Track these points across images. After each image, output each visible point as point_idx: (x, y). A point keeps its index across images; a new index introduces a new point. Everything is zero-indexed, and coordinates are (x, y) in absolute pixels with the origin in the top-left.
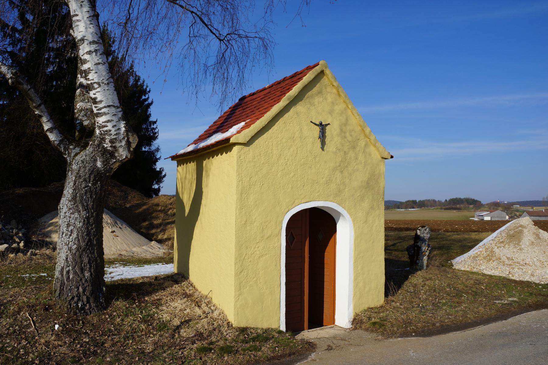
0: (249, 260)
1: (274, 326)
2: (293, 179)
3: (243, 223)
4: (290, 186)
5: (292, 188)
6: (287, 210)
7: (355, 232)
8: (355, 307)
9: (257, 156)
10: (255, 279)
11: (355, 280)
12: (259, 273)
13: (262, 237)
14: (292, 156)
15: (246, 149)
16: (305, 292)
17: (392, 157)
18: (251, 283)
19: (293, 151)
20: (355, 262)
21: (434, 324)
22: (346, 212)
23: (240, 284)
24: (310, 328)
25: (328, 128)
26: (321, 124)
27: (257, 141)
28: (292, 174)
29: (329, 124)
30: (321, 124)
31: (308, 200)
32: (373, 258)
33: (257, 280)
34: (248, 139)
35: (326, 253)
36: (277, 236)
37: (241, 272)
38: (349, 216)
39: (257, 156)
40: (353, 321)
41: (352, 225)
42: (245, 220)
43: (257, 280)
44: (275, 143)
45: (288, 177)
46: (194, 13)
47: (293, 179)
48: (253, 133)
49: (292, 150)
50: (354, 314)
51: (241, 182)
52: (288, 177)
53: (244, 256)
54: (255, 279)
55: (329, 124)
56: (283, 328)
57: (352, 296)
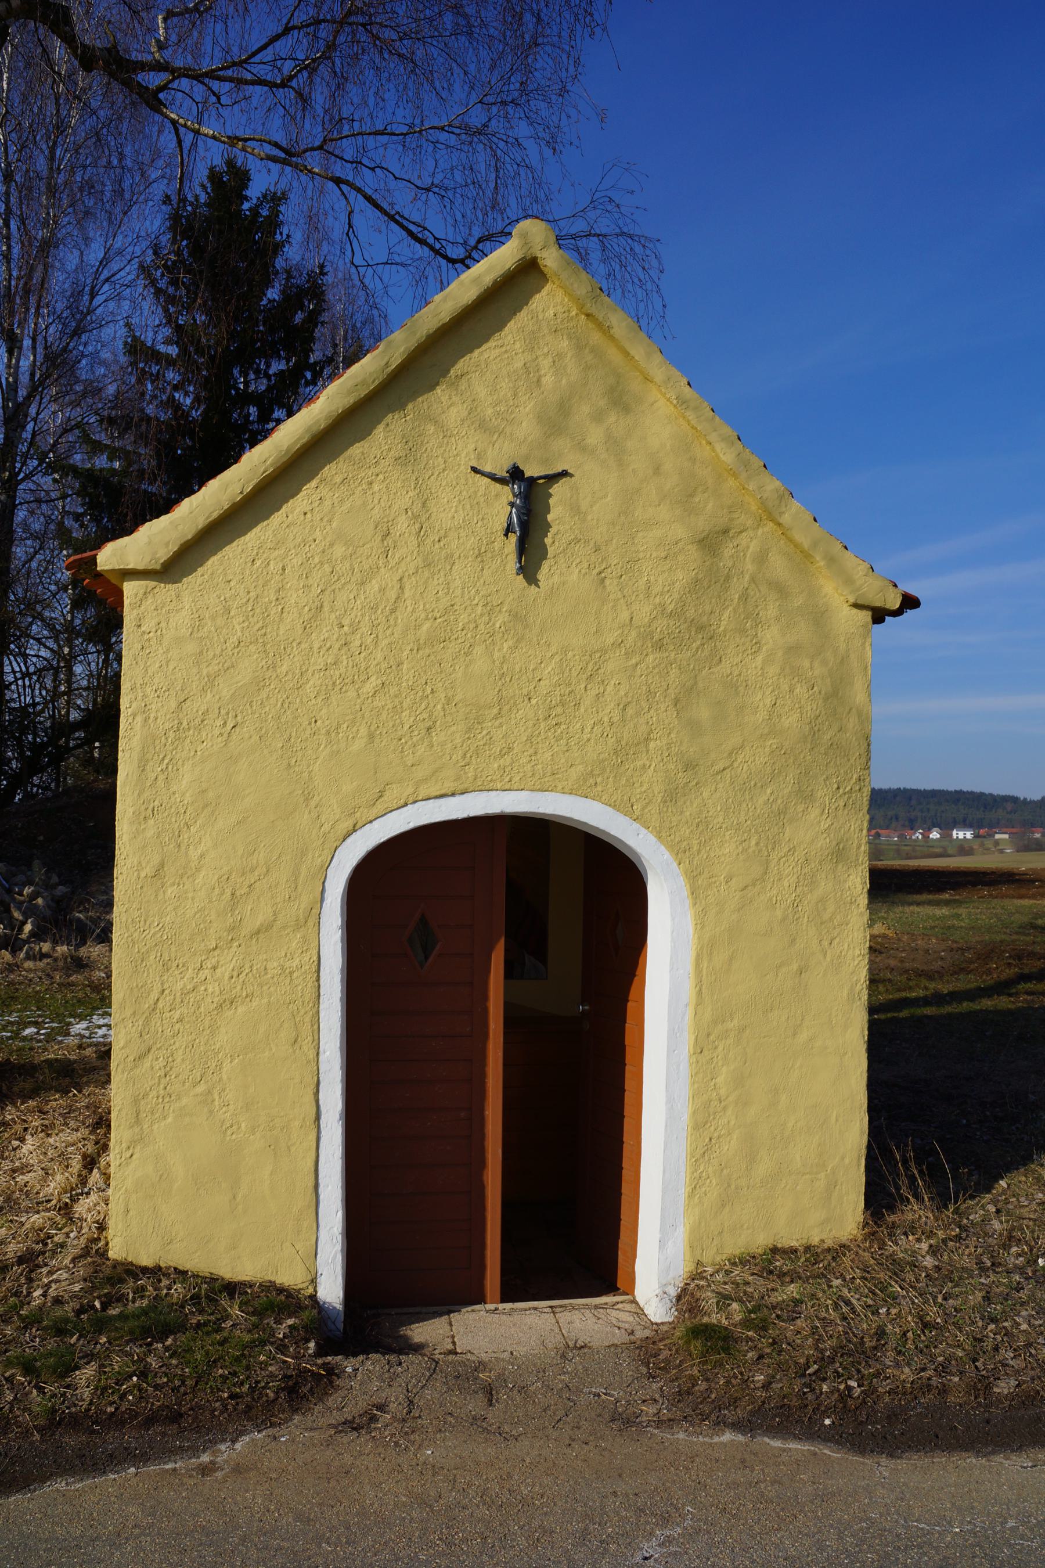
0: (177, 1015)
1: (290, 1277)
2: (378, 703)
3: (148, 871)
4: (363, 731)
5: (371, 737)
6: (348, 824)
7: (701, 924)
8: (695, 1242)
9: (213, 618)
10: (201, 1088)
11: (699, 1125)
12: (220, 1067)
13: (232, 929)
14: (374, 609)
15: (165, 591)
16: (489, 1156)
17: (910, 602)
18: (185, 1101)
19: (382, 590)
20: (699, 1050)
21: (982, 1386)
22: (652, 839)
23: (136, 1101)
24: (510, 1293)
25: (558, 491)
26: (516, 474)
27: (213, 561)
28: (374, 682)
29: (564, 474)
30: (516, 474)
31: (449, 786)
32: (803, 1036)
33: (209, 1092)
34: (164, 554)
35: (629, 1004)
36: (298, 927)
37: (141, 1057)
38: (667, 855)
39: (213, 618)
40: (679, 1298)
41: (686, 892)
42: (156, 860)
43: (209, 1092)
44: (297, 561)
45: (352, 694)
46: (347, 183)
47: (378, 703)
48: (188, 531)
49: (375, 585)
50: (691, 1267)
51: (139, 719)
52: (352, 694)
53: (154, 995)
54: (201, 1088)
55: (564, 474)
56: (331, 1290)
57: (683, 1192)
